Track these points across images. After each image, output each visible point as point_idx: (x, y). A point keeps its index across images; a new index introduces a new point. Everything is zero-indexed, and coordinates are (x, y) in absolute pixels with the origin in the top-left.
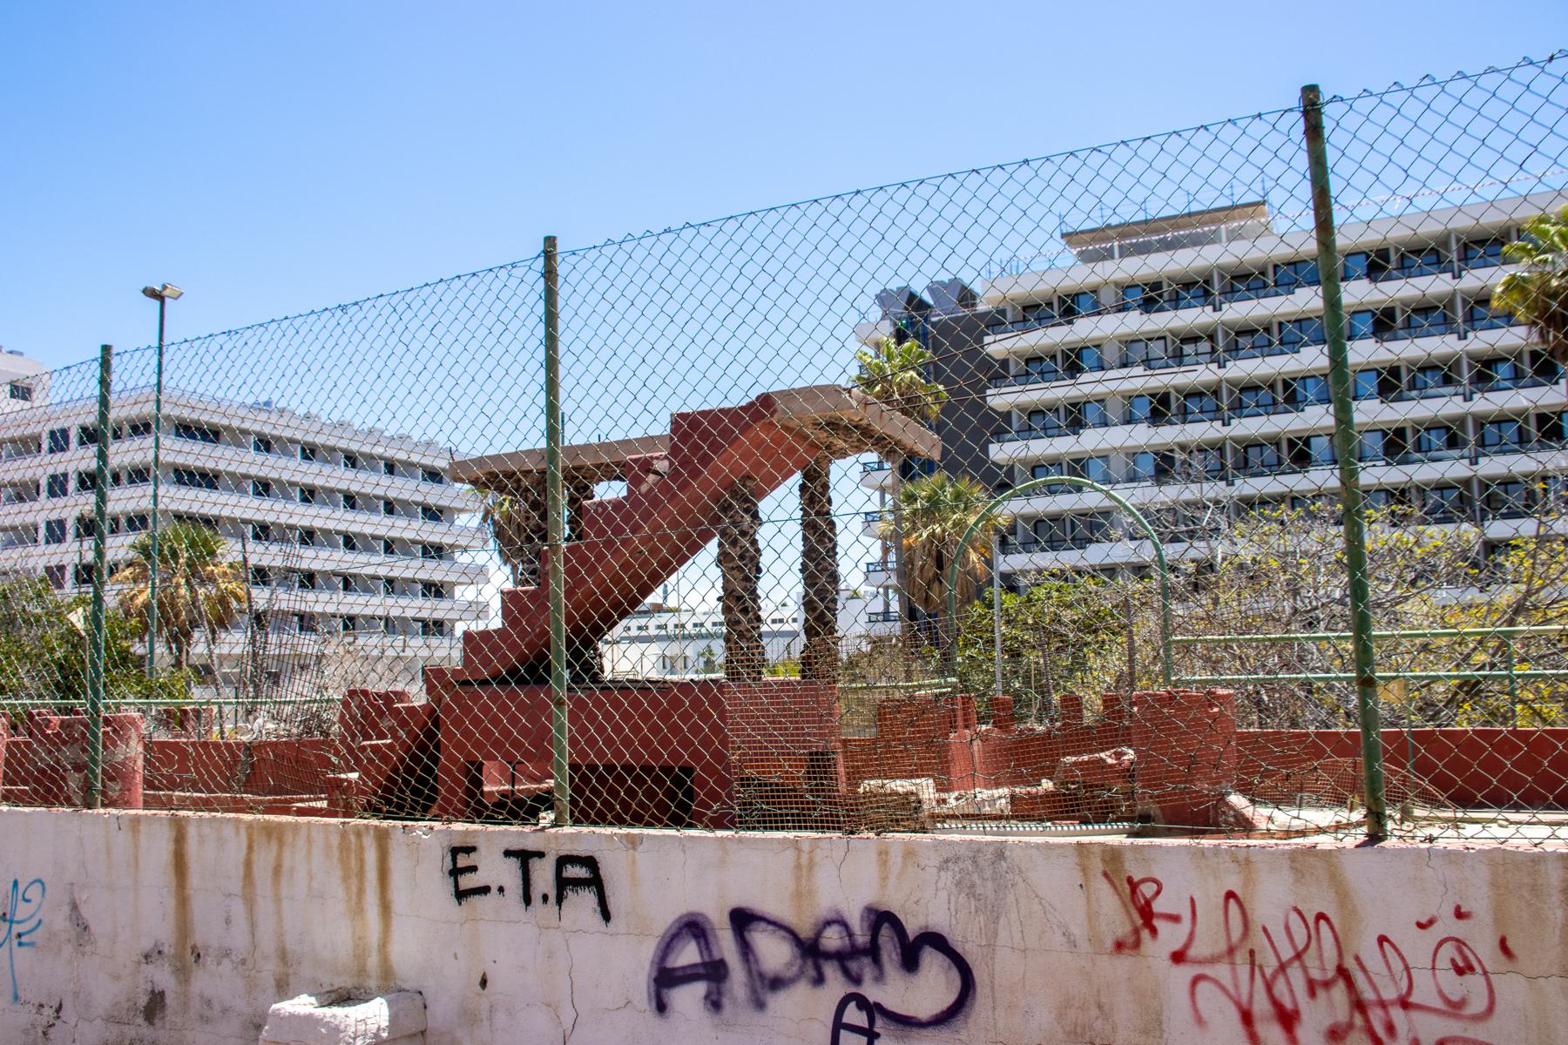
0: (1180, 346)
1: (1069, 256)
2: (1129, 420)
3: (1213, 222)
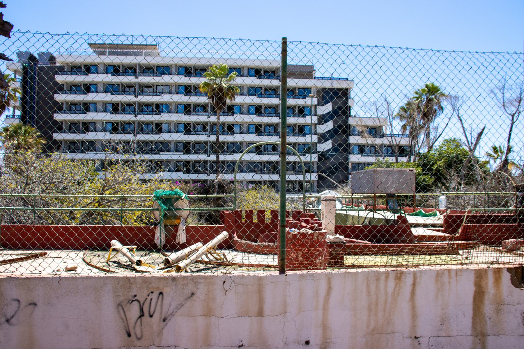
0: (125, 89)
1: (90, 51)
2: (105, 111)
3: (140, 49)
